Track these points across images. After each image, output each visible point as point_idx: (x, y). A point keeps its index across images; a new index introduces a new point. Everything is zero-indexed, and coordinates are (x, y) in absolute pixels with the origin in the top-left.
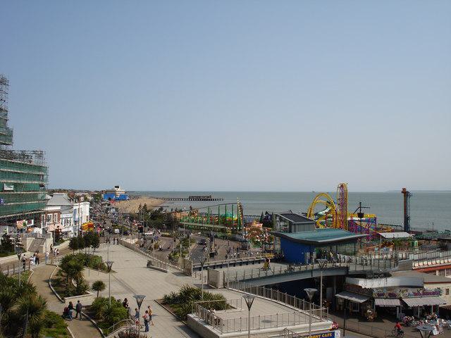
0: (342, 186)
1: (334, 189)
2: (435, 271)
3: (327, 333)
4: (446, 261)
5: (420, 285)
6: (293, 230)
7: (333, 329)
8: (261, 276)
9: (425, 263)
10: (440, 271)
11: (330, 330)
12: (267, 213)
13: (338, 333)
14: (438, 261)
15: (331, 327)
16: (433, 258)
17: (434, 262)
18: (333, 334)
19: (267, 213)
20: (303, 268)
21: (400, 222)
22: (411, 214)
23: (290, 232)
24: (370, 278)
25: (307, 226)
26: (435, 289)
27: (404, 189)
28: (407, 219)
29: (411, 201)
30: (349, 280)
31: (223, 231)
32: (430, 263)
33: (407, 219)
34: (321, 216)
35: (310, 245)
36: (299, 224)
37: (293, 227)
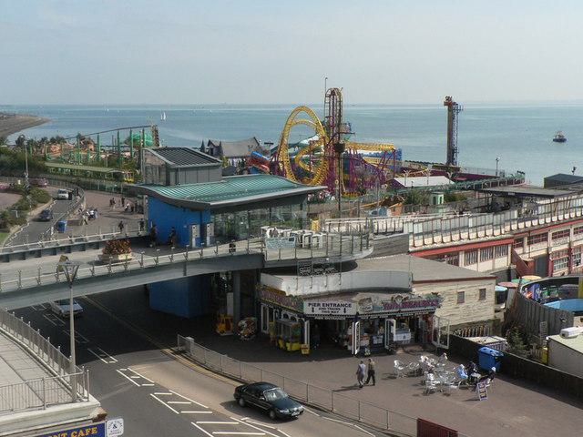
0: (333, 93)
1: (317, 102)
2: (457, 254)
3: (84, 429)
4: (481, 234)
5: (405, 285)
6: (172, 180)
7: (101, 417)
8: (145, 265)
9: (437, 238)
10: (467, 252)
11: (94, 420)
12: (210, 143)
13: (115, 430)
14: (464, 235)
15: (95, 414)
16: (455, 229)
17: (456, 237)
18: (101, 429)
19: (210, 143)
20: (179, 257)
21: (443, 160)
22: (460, 137)
23: (168, 184)
24: (305, 275)
25: (205, 172)
26: (428, 296)
27: (449, 99)
28: (452, 152)
29: (460, 117)
30: (266, 279)
31: (117, 177)
32: (447, 239)
33: (452, 152)
34: (304, 146)
35: (199, 210)
36: (182, 169)
37: (172, 174)
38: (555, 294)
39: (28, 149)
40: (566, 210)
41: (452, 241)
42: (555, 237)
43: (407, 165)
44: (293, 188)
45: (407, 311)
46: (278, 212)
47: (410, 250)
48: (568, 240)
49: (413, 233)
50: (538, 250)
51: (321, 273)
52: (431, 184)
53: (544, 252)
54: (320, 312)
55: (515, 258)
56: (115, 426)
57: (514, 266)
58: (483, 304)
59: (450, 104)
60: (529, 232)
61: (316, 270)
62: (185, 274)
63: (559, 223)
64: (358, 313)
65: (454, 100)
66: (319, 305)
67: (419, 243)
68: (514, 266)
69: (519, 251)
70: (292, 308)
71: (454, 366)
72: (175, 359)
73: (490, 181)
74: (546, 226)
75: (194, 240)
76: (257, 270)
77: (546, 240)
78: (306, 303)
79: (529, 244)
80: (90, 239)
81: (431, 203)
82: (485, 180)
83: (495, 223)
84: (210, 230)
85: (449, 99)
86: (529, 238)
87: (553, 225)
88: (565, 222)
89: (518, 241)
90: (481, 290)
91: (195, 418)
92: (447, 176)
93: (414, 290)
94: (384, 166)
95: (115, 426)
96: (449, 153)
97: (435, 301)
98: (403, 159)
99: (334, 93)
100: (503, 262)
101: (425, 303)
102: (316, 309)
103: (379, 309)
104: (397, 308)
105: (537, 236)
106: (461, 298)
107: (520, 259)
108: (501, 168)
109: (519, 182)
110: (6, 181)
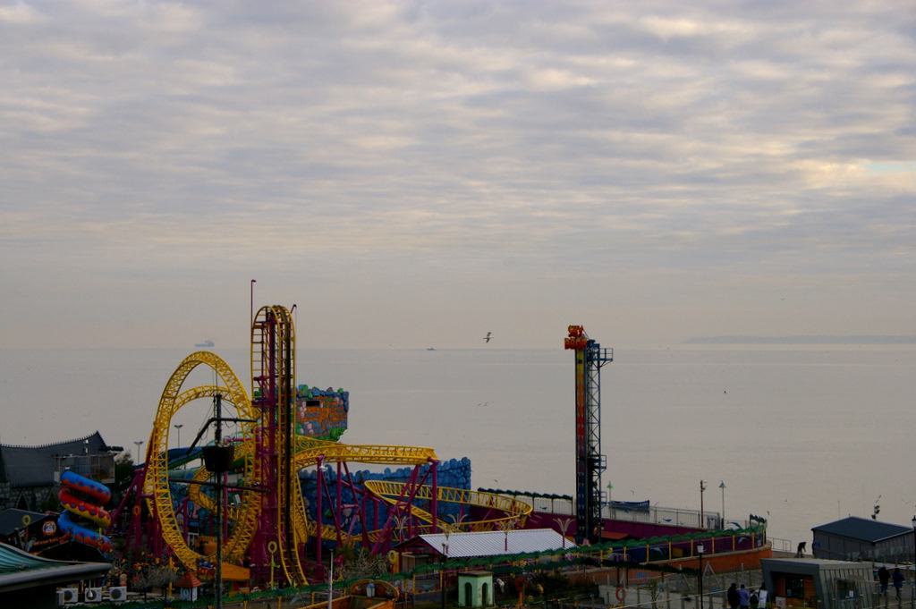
0: (271, 320)
27: (575, 332)
28: (588, 463)
29: (607, 379)
33: (588, 463)
39: (235, 510)
43: (483, 501)
52: (514, 549)
59: (583, 348)
65: (590, 334)
71: (889, 587)
73: (677, 538)
82: (655, 539)
85: (575, 332)
92: (558, 530)
94: (412, 500)
96: (579, 468)
98: (474, 487)
108: (712, 508)
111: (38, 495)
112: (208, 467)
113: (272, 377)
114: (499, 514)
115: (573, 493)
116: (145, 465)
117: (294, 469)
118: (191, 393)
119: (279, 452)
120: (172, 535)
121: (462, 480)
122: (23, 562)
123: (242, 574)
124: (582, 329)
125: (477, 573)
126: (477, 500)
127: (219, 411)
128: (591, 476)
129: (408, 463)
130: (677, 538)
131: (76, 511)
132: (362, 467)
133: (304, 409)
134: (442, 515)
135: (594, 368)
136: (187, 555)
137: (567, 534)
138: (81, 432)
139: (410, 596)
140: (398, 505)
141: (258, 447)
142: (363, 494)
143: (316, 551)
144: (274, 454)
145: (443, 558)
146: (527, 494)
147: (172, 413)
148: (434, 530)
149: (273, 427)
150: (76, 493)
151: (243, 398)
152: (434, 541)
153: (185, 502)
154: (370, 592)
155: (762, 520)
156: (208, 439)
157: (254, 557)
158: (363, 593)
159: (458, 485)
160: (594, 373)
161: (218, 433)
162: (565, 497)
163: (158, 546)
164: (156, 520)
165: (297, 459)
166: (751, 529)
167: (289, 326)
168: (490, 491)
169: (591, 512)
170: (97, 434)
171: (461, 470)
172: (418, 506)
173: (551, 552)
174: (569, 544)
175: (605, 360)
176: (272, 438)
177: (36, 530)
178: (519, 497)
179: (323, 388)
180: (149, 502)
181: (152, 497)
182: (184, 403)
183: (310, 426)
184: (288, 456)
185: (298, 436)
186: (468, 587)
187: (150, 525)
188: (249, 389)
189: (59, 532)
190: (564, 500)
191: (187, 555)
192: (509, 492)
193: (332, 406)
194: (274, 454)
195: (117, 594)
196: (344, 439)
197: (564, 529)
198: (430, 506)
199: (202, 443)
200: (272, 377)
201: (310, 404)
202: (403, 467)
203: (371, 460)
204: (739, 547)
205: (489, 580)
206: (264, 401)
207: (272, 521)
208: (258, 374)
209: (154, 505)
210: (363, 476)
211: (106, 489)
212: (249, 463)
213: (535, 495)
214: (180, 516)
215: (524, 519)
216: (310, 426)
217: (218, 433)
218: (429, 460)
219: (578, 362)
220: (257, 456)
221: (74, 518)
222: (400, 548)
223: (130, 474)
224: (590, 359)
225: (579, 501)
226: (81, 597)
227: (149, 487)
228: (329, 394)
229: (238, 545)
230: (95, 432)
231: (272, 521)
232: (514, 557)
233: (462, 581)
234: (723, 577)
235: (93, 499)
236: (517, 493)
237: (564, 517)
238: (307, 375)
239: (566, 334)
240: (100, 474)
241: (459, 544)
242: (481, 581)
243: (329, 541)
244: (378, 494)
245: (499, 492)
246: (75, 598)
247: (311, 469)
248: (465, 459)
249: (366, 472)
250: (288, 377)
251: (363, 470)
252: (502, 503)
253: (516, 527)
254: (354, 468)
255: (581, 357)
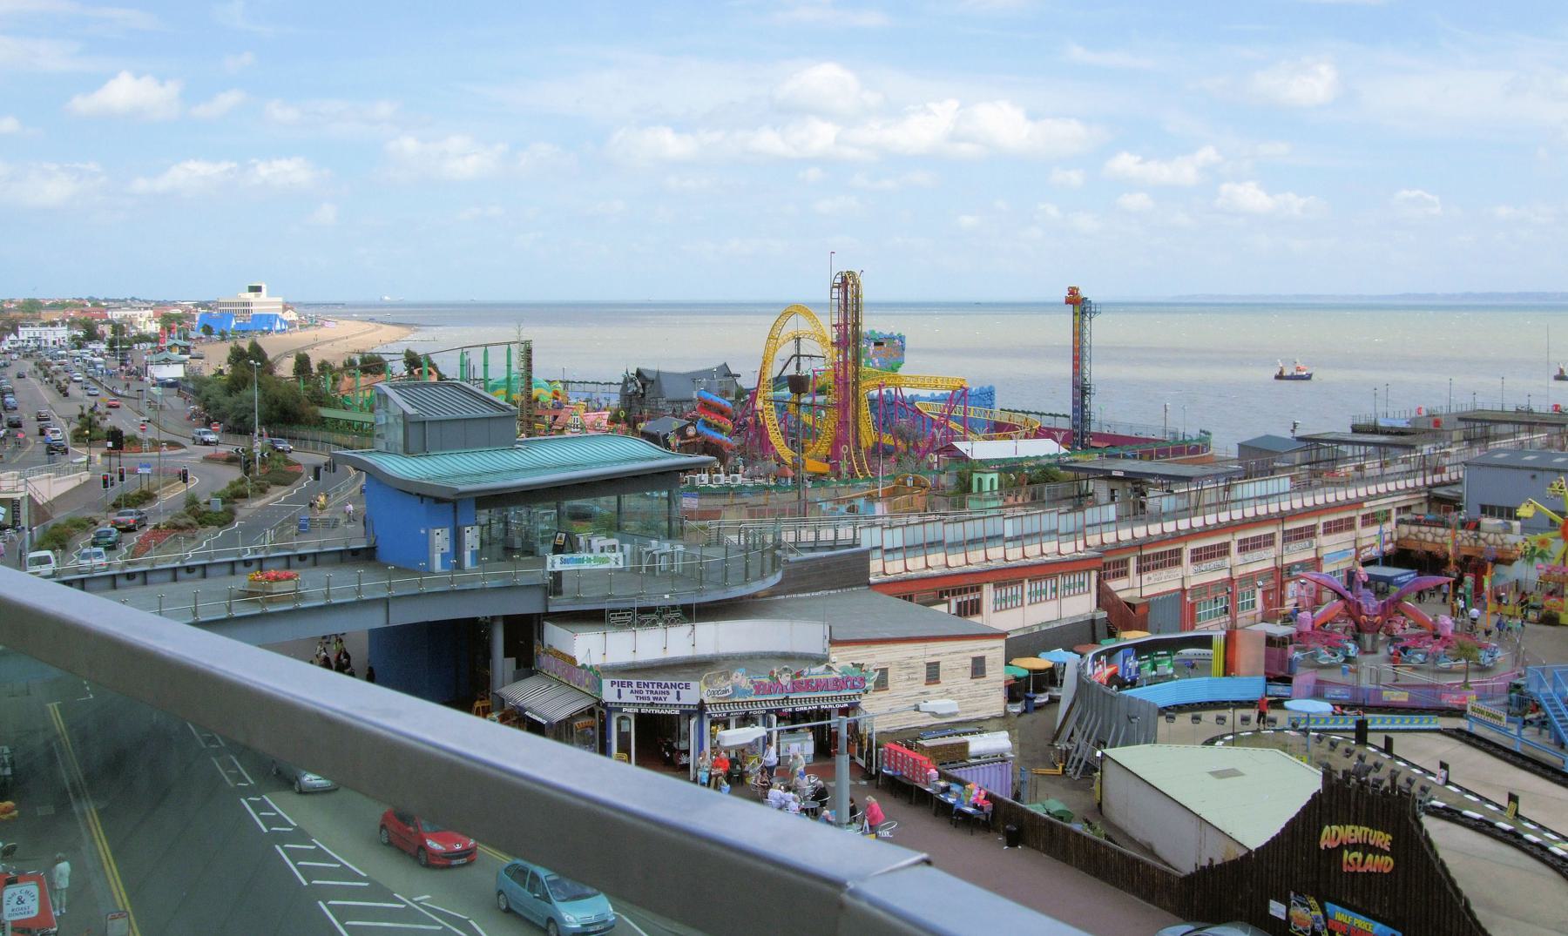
0: (844, 283)
27: (1073, 291)
28: (1081, 390)
33: (1081, 390)
38: (1166, 667)
40: (1222, 505)
41: (967, 564)
42: (1198, 556)
43: (1004, 418)
44: (652, 459)
45: (804, 701)
46: (603, 505)
47: (872, 579)
48: (1177, 572)
49: (881, 547)
50: (1160, 583)
51: (654, 623)
53: (1176, 585)
54: (632, 699)
55: (1105, 598)
56: (20, 901)
57: (1104, 614)
58: (982, 685)
59: (1077, 303)
60: (1141, 547)
61: (644, 617)
62: (388, 622)
63: (1206, 531)
64: (702, 701)
66: (630, 684)
67: (895, 567)
68: (1104, 614)
69: (1114, 585)
70: (587, 690)
72: (1053, 815)
74: (1178, 536)
75: (438, 557)
76: (539, 615)
77: (1178, 562)
78: (606, 683)
79: (1140, 571)
80: (195, 557)
81: (975, 488)
82: (1127, 447)
83: (1062, 530)
84: (471, 538)
85: (1073, 291)
86: (1140, 559)
87: (1192, 534)
88: (1220, 529)
89: (1108, 564)
90: (974, 659)
91: (327, 893)
92: (1055, 440)
93: (833, 658)
95: (20, 901)
97: (855, 680)
99: (847, 283)
100: (1080, 605)
101: (839, 684)
102: (625, 691)
103: (745, 692)
104: (782, 691)
105: (1160, 557)
106: (933, 673)
107: (1119, 600)
108: (1171, 426)
109: (1196, 450)
110: (1527, 461)
111: (684, 407)
112: (792, 391)
113: (846, 324)
114: (1013, 428)
115: (1069, 412)
116: (757, 389)
117: (862, 392)
118: (790, 335)
119: (851, 380)
120: (776, 438)
121: (989, 402)
122: (661, 454)
123: (824, 468)
124: (1078, 289)
125: (984, 470)
126: (1000, 417)
127: (799, 349)
128: (1083, 401)
129: (946, 389)
130: (1144, 448)
131: (708, 419)
132: (914, 392)
133: (872, 347)
134: (969, 427)
135: (1087, 318)
136: (786, 454)
137: (1063, 443)
138: (713, 364)
139: (943, 486)
140: (939, 420)
141: (836, 376)
142: (914, 412)
143: (879, 451)
144: (846, 382)
145: (966, 458)
146: (1036, 413)
147: (775, 350)
148: (965, 439)
149: (846, 362)
150: (706, 406)
151: (824, 340)
152: (961, 446)
153: (786, 415)
154: (910, 483)
155: (1208, 433)
156: (791, 371)
157: (833, 458)
158: (905, 483)
159: (985, 405)
160: (1087, 323)
161: (798, 366)
162: (1065, 416)
163: (766, 445)
164: (764, 427)
165: (864, 385)
166: (1199, 440)
167: (858, 286)
168: (1009, 410)
169: (1083, 428)
170: (725, 364)
171: (987, 395)
172: (955, 421)
173: (1048, 456)
174: (1063, 450)
175: (1095, 313)
176: (845, 369)
177: (681, 432)
178: (1030, 416)
179: (887, 333)
180: (760, 415)
181: (762, 411)
182: (784, 343)
183: (877, 361)
184: (856, 384)
185: (865, 368)
186: (980, 480)
187: (761, 430)
188: (832, 335)
189: (697, 435)
190: (1063, 418)
191: (786, 454)
192: (1023, 412)
193: (891, 346)
194: (846, 382)
195: (734, 480)
196: (901, 372)
197: (1060, 439)
198: (964, 421)
199: (786, 373)
200: (846, 324)
201: (876, 344)
202: (944, 392)
203: (919, 386)
204: (1190, 453)
205: (995, 476)
206: (842, 343)
207: (846, 428)
208: (835, 322)
209: (763, 417)
210: (913, 399)
211: (729, 404)
212: (830, 387)
213: (1042, 414)
214: (783, 425)
215: (1033, 432)
216: (877, 361)
217: (798, 366)
218: (961, 387)
219: (1075, 314)
220: (835, 382)
221: (708, 425)
222: (938, 452)
223: (746, 397)
224: (1083, 313)
225: (1075, 418)
226: (710, 482)
227: (759, 404)
228: (891, 338)
229: (823, 447)
230: (722, 363)
231: (846, 428)
232: (1021, 460)
233: (975, 477)
234: (967, 564)
235: (722, 412)
236: (1029, 413)
237: (1060, 431)
238: (871, 324)
239: (1066, 293)
240: (725, 394)
241: (980, 449)
242: (989, 477)
243: (889, 446)
244: (924, 411)
245: (1016, 411)
246: (706, 482)
247: (875, 393)
248: (991, 387)
249: (917, 395)
250: (856, 325)
251: (914, 394)
252: (1017, 419)
253: (1027, 437)
254: (907, 392)
255: (1077, 310)
